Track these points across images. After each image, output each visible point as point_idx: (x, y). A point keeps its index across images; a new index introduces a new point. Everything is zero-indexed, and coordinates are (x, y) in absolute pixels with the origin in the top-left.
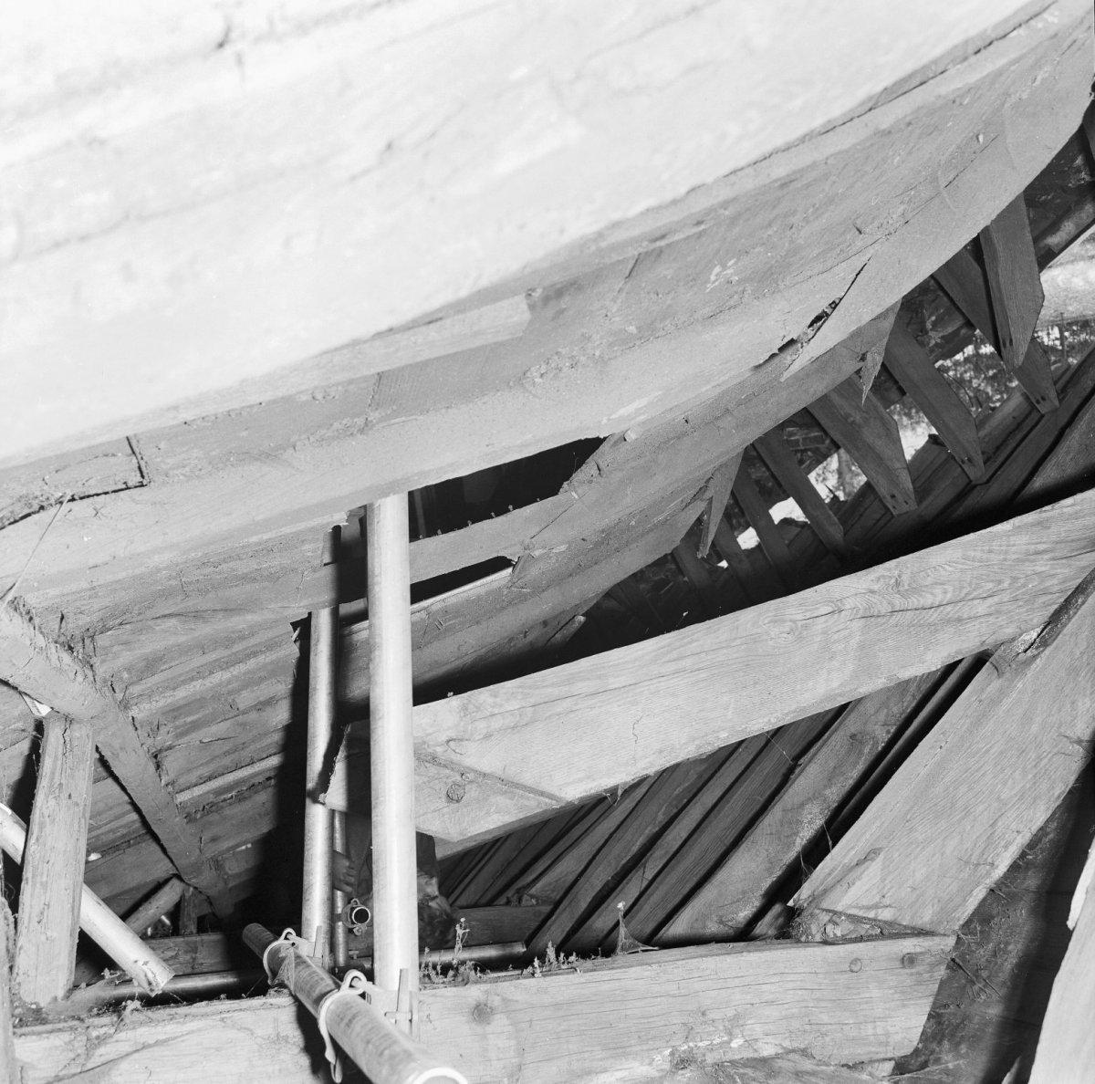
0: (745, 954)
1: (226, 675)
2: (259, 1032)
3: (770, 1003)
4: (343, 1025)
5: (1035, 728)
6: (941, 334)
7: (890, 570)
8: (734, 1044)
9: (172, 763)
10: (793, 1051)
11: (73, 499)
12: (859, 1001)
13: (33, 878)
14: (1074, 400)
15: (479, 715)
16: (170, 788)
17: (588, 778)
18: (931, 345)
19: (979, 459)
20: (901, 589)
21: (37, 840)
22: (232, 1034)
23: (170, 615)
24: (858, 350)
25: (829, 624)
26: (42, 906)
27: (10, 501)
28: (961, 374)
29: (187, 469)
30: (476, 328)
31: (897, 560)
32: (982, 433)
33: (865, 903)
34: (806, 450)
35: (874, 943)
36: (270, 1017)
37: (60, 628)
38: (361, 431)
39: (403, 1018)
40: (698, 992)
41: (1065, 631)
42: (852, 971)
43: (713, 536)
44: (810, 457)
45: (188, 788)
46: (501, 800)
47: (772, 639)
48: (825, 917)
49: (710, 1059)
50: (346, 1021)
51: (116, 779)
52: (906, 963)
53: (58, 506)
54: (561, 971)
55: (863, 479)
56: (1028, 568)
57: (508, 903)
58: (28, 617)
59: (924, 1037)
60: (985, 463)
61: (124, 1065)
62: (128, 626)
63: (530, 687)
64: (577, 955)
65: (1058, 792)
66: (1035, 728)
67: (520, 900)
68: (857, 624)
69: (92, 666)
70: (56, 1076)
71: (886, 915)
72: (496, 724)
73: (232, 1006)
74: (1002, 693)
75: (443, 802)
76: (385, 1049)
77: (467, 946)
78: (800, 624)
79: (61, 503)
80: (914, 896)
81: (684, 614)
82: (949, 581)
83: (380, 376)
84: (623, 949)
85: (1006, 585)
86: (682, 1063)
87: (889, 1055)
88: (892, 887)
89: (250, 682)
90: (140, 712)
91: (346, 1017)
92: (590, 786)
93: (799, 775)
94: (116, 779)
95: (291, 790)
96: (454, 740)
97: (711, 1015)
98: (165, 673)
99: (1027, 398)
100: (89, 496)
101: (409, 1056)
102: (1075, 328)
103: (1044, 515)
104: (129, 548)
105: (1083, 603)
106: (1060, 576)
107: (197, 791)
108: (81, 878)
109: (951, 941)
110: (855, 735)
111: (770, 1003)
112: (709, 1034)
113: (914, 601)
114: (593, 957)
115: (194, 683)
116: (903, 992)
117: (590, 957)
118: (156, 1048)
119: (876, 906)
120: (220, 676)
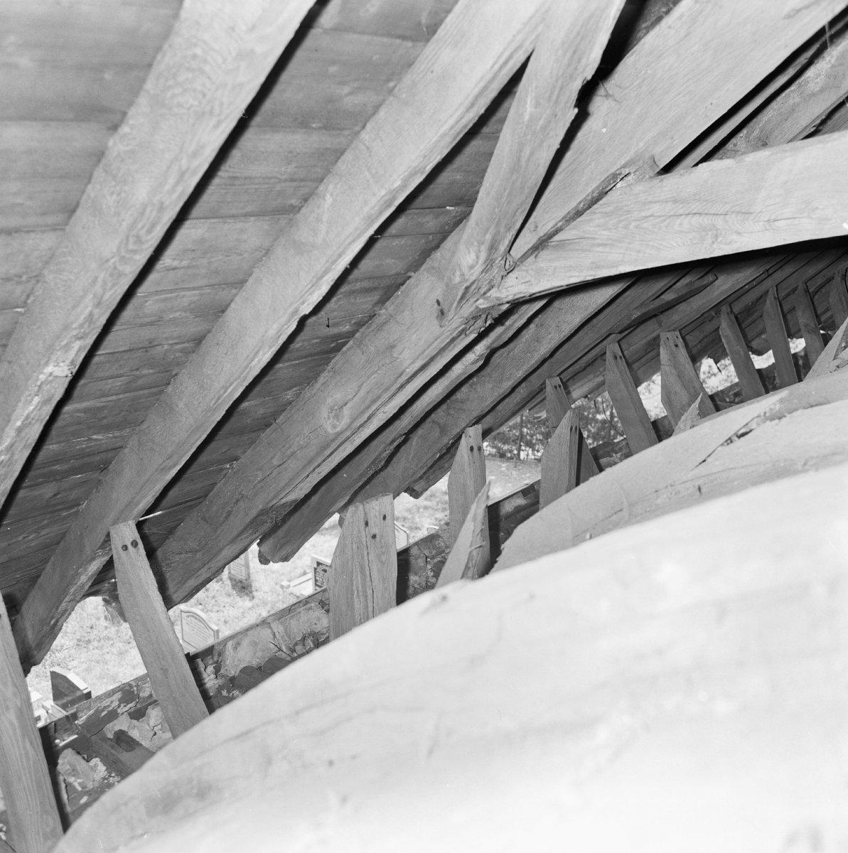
14: (535, 381)
18: (620, 454)
19: (609, 356)
20: (715, 232)
28: (593, 443)
32: (600, 379)
41: (598, 182)
44: (728, 397)
60: (605, 353)
65: (631, 58)
78: (805, 215)
85: (633, 224)
99: (568, 393)
102: (509, 455)
105: (580, 202)
113: (706, 221)
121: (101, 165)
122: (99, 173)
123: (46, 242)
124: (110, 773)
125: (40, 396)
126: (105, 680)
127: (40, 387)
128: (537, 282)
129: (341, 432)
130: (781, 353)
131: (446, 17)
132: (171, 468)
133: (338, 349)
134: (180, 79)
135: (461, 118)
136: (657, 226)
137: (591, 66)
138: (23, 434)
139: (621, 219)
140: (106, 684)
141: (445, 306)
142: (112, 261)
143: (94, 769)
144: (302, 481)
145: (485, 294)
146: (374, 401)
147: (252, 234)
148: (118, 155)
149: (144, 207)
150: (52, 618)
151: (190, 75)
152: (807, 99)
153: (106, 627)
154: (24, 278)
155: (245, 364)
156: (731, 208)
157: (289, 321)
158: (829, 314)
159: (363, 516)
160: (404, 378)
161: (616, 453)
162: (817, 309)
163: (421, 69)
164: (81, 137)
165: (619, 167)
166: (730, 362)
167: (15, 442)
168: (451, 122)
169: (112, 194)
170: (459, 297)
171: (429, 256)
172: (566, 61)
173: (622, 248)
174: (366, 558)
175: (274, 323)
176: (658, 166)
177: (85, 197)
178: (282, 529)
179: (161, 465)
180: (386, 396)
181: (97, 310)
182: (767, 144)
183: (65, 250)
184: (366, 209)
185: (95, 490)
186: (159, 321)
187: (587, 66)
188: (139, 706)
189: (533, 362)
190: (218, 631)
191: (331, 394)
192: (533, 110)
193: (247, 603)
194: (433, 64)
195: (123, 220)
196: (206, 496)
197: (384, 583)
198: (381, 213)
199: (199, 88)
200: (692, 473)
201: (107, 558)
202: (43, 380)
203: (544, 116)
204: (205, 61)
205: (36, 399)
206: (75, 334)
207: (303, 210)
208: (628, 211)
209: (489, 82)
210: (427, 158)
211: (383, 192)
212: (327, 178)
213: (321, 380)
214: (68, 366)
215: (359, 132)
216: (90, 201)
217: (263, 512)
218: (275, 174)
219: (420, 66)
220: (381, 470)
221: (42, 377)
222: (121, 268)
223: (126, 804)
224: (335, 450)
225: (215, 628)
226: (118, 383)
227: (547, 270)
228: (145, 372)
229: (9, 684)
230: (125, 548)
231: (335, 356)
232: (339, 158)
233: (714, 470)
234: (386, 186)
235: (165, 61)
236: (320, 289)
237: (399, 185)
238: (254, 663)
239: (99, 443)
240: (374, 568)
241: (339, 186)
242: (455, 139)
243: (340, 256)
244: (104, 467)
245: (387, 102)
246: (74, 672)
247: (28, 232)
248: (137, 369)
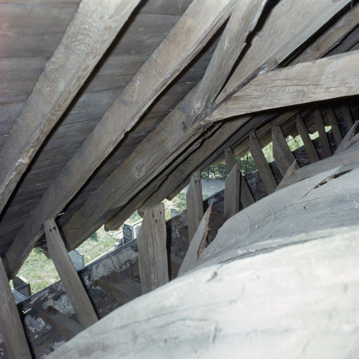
5: (269, 40)
6: (252, 181)
7: (306, 100)
14: (220, 150)
18: (255, 178)
19: (251, 138)
20: (303, 93)
24: (294, 177)
25: (332, 84)
32: (247, 147)
34: (301, 154)
41: (253, 71)
43: (352, 127)
56: (259, 94)
66: (269, 40)
68: (321, 83)
74: (277, 53)
78: (343, 86)
82: (287, 93)
85: (268, 89)
99: (234, 153)
102: (204, 176)
103: (251, 110)
105: (245, 80)
106: (250, 89)
110: (318, 50)
113: (300, 88)
121: (42, 74)
122: (41, 78)
123: (18, 107)
124: (47, 324)
125: (16, 172)
126: (35, 278)
127: (16, 168)
128: (226, 114)
129: (142, 178)
130: (322, 132)
131: (189, 5)
132: (70, 197)
133: (140, 142)
134: (78, 38)
135: (196, 48)
136: (279, 90)
137: (253, 26)
138: (8, 188)
139: (262, 87)
140: (36, 280)
141: (187, 125)
142: (49, 115)
143: (40, 323)
144: (125, 198)
145: (203, 119)
146: (156, 164)
147: (104, 98)
148: (51, 70)
149: (63, 92)
150: (19, 260)
151: (83, 37)
152: (336, 30)
153: (35, 255)
154: (9, 122)
155: (102, 153)
156: (311, 83)
157: (121, 134)
158: (340, 115)
159: (152, 213)
160: (169, 154)
161: (254, 178)
162: (336, 113)
163: (178, 27)
164: (34, 63)
165: (261, 65)
167: (5, 190)
168: (192, 50)
169: (48, 87)
170: (193, 121)
171: (178, 102)
172: (243, 25)
173: (263, 99)
174: (153, 230)
175: (115, 135)
176: (277, 63)
177: (35, 88)
178: (114, 218)
179: (66, 195)
180: (161, 162)
181: (41, 136)
183: (26, 110)
184: (155, 87)
185: (36, 206)
186: (65, 136)
187: (251, 26)
188: (57, 294)
189: (220, 143)
190: (83, 256)
191: (136, 162)
192: (228, 45)
193: (95, 243)
194: (183, 25)
195: (53, 98)
196: (83, 205)
197: (161, 240)
198: (161, 88)
199: (87, 42)
200: (301, 200)
201: (42, 234)
202: (17, 165)
203: (232, 47)
204: (90, 31)
205: (14, 173)
206: (31, 146)
207: (127, 87)
208: (266, 84)
209: (208, 33)
210: (181, 65)
211: (162, 80)
212: (137, 73)
213: (133, 155)
214: (28, 159)
215: (151, 54)
216: (37, 90)
217: (108, 212)
218: (115, 73)
219: (178, 26)
220: (156, 191)
221: (17, 164)
222: (52, 118)
223: (69, 352)
224: (139, 185)
225: (82, 254)
226: (47, 162)
227: (231, 109)
228: (59, 157)
229: (5, 292)
230: (51, 230)
231: (138, 145)
232: (142, 65)
233: (310, 199)
234: (164, 77)
235: (71, 30)
236: (134, 120)
237: (169, 77)
238: (105, 274)
239: (38, 187)
240: (157, 234)
241: (142, 77)
242: (193, 56)
243: (143, 107)
244: (41, 196)
245: (164, 41)
246: (22, 275)
247: (10, 103)
248: (55, 156)
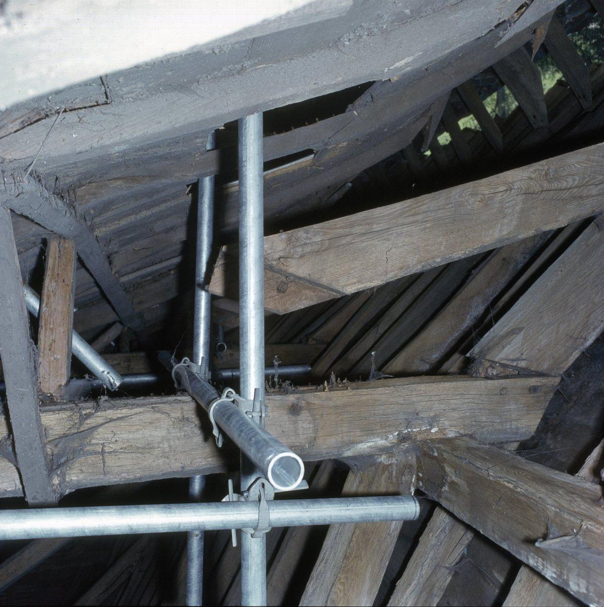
0: (442, 383)
1: (148, 213)
2: (173, 415)
3: (454, 410)
4: (224, 419)
8: (433, 431)
9: (118, 262)
10: (465, 435)
11: (65, 111)
12: (503, 410)
13: (45, 325)
15: (298, 244)
16: (117, 275)
17: (359, 282)
18: (566, 23)
20: (548, 177)
21: (47, 305)
22: (158, 415)
23: (118, 179)
26: (51, 341)
27: (27, 111)
29: (134, 94)
30: (318, 10)
31: (547, 160)
33: (511, 357)
35: (515, 380)
36: (181, 407)
37: (56, 184)
38: (239, 73)
39: (256, 415)
40: (415, 402)
42: (501, 394)
45: (126, 274)
46: (309, 293)
47: (470, 205)
48: (487, 364)
49: (419, 438)
50: (226, 417)
51: (87, 270)
52: (531, 391)
53: (57, 115)
54: (338, 388)
55: (514, 105)
57: (300, 342)
58: (38, 180)
59: (538, 431)
60: (593, 99)
61: (100, 430)
62: (94, 184)
63: (328, 228)
64: (347, 379)
67: (307, 340)
68: (520, 198)
69: (74, 207)
70: (64, 434)
71: (523, 364)
72: (308, 249)
73: (158, 400)
75: (275, 293)
76: (252, 437)
77: (280, 366)
78: (487, 196)
79: (59, 113)
80: (539, 355)
81: (413, 185)
83: (254, 39)
84: (373, 377)
86: (403, 439)
87: (517, 439)
88: (527, 349)
89: (161, 217)
90: (100, 232)
91: (223, 411)
92: (359, 287)
93: (472, 280)
94: (87, 270)
95: (186, 280)
96: (283, 258)
97: (421, 415)
98: (114, 211)
100: (75, 109)
101: (266, 444)
104: (100, 143)
107: (131, 276)
108: (71, 326)
109: (558, 380)
111: (454, 410)
112: (420, 425)
113: (555, 185)
114: (356, 381)
115: (131, 217)
116: (528, 406)
117: (355, 381)
118: (117, 421)
119: (517, 359)
120: (145, 213)
166: (491, 115)
182: (503, 260)
